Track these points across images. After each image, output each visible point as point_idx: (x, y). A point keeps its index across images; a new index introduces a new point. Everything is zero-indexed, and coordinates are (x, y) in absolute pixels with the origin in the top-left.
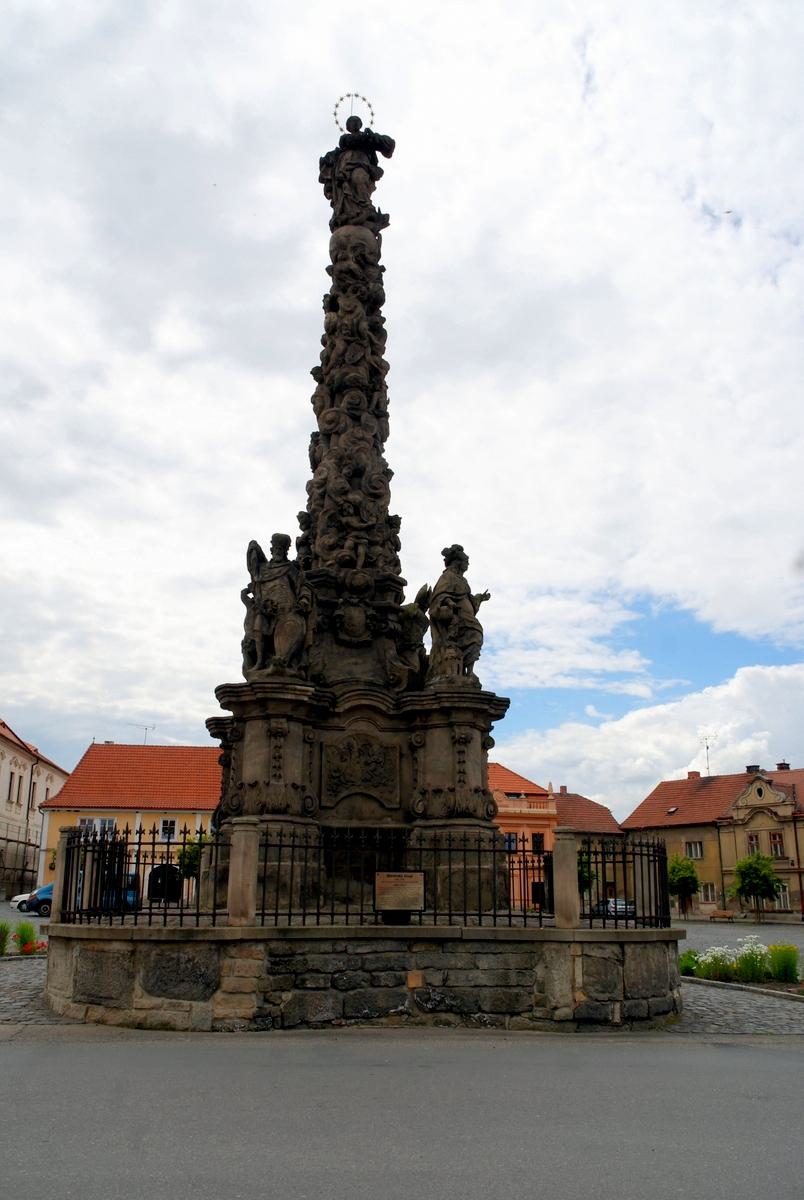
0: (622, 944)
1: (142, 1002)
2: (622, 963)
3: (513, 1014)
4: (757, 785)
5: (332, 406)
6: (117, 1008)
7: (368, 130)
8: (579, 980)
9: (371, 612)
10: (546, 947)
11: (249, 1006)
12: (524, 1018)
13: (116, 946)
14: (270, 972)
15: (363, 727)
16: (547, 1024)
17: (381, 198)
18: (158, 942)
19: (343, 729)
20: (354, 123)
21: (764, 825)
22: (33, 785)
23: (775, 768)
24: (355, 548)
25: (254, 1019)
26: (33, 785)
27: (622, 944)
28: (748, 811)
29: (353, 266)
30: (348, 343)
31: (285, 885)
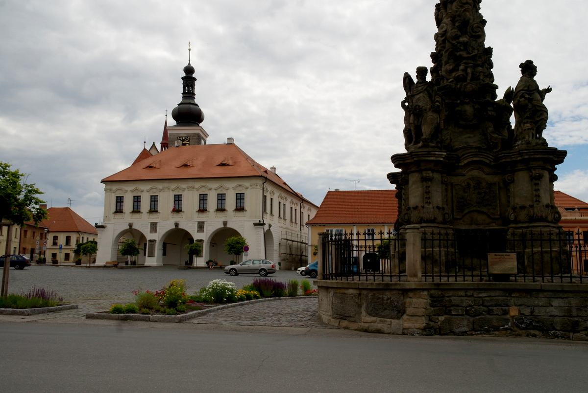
1: (366, 319)
6: (354, 322)
11: (421, 323)
13: (351, 291)
15: (476, 173)
18: (371, 290)
19: (464, 175)
22: (302, 213)
24: (465, 70)
25: (424, 329)
26: (302, 213)
31: (436, 260)
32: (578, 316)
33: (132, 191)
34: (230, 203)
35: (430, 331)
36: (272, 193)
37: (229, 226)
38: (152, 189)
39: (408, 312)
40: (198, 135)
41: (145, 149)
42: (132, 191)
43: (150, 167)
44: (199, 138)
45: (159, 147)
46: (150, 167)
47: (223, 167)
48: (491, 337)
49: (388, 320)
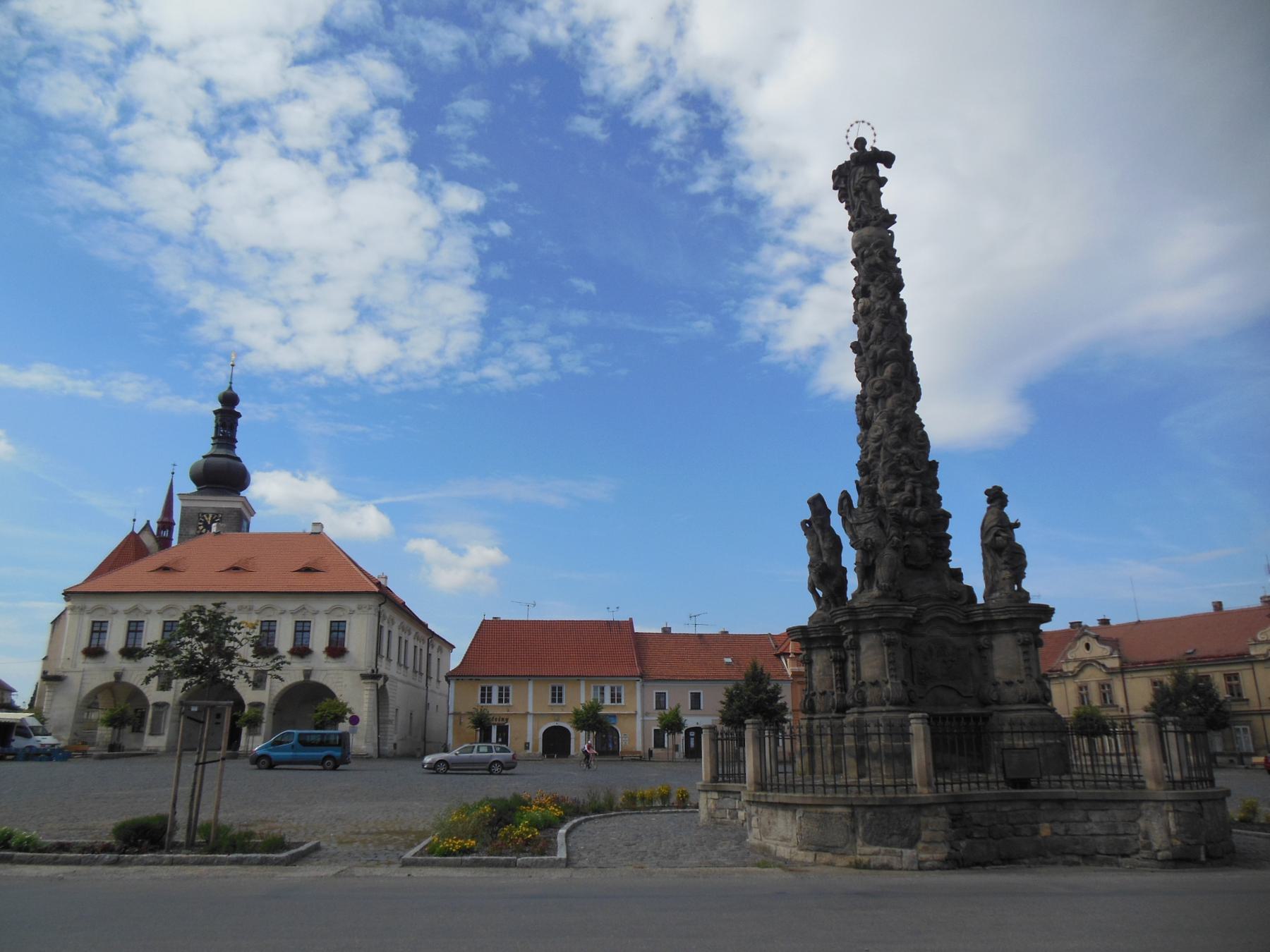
0: (1199, 802)
1: (865, 851)
2: (1202, 816)
3: (1124, 856)
4: (1085, 640)
5: (875, 375)
6: (844, 854)
7: (874, 149)
8: (1173, 830)
9: (931, 542)
10: (1143, 806)
11: (941, 852)
12: (1133, 859)
13: (837, 810)
14: (954, 827)
16: (1153, 863)
17: (889, 199)
18: (870, 807)
20: (860, 143)
21: (1092, 677)
22: (429, 655)
23: (1096, 624)
24: (913, 491)
25: (946, 860)
26: (429, 655)
27: (1199, 802)
28: (1076, 664)
29: (879, 261)
30: (885, 324)
32: (1126, 834)
33: (128, 612)
34: (319, 639)
35: (956, 862)
36: (392, 622)
37: (312, 679)
38: (136, 609)
39: (923, 837)
40: (239, 512)
41: (133, 533)
42: (128, 612)
43: (165, 569)
44: (240, 519)
45: (155, 527)
46: (165, 569)
47: (304, 575)
48: (450, 872)
49: (898, 850)
